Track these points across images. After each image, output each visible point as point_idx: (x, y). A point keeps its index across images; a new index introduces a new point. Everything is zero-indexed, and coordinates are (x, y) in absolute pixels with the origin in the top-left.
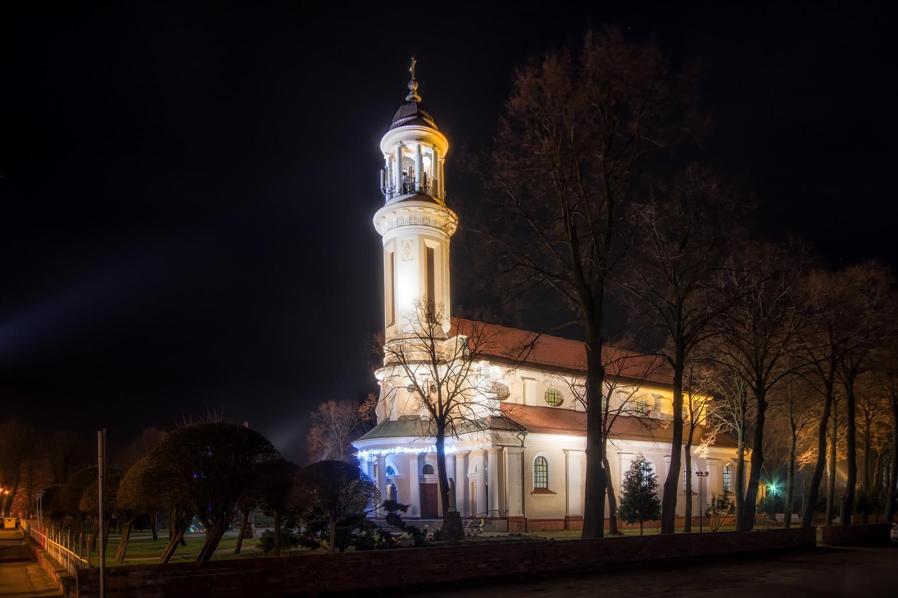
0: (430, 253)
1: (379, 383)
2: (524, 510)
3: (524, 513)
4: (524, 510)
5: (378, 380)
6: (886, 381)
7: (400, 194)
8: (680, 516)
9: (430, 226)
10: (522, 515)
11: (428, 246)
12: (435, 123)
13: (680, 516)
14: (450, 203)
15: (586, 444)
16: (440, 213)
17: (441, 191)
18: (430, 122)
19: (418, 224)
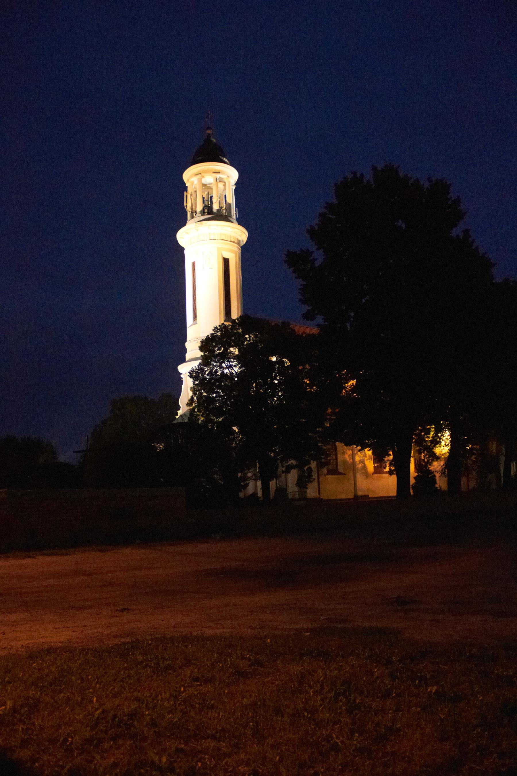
0: (226, 262)
1: (182, 376)
2: (319, 490)
3: (319, 494)
4: (319, 490)
5: (181, 374)
6: (469, 465)
7: (200, 215)
8: (370, 496)
9: (226, 240)
10: (318, 495)
11: (225, 257)
12: (228, 160)
13: (370, 496)
14: (241, 221)
15: (241, 275)
16: (236, 230)
17: (234, 212)
18: (224, 159)
19: (216, 239)
